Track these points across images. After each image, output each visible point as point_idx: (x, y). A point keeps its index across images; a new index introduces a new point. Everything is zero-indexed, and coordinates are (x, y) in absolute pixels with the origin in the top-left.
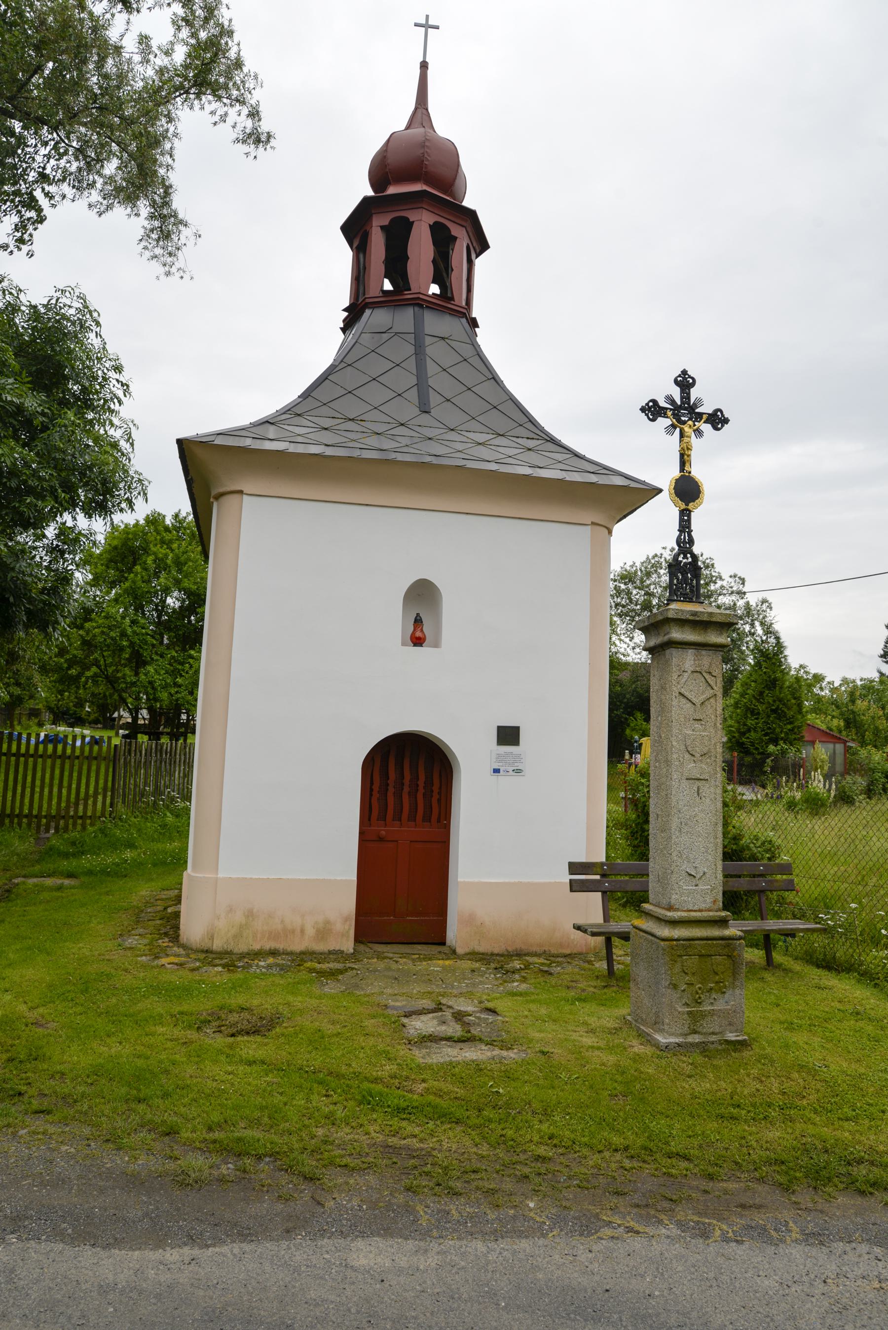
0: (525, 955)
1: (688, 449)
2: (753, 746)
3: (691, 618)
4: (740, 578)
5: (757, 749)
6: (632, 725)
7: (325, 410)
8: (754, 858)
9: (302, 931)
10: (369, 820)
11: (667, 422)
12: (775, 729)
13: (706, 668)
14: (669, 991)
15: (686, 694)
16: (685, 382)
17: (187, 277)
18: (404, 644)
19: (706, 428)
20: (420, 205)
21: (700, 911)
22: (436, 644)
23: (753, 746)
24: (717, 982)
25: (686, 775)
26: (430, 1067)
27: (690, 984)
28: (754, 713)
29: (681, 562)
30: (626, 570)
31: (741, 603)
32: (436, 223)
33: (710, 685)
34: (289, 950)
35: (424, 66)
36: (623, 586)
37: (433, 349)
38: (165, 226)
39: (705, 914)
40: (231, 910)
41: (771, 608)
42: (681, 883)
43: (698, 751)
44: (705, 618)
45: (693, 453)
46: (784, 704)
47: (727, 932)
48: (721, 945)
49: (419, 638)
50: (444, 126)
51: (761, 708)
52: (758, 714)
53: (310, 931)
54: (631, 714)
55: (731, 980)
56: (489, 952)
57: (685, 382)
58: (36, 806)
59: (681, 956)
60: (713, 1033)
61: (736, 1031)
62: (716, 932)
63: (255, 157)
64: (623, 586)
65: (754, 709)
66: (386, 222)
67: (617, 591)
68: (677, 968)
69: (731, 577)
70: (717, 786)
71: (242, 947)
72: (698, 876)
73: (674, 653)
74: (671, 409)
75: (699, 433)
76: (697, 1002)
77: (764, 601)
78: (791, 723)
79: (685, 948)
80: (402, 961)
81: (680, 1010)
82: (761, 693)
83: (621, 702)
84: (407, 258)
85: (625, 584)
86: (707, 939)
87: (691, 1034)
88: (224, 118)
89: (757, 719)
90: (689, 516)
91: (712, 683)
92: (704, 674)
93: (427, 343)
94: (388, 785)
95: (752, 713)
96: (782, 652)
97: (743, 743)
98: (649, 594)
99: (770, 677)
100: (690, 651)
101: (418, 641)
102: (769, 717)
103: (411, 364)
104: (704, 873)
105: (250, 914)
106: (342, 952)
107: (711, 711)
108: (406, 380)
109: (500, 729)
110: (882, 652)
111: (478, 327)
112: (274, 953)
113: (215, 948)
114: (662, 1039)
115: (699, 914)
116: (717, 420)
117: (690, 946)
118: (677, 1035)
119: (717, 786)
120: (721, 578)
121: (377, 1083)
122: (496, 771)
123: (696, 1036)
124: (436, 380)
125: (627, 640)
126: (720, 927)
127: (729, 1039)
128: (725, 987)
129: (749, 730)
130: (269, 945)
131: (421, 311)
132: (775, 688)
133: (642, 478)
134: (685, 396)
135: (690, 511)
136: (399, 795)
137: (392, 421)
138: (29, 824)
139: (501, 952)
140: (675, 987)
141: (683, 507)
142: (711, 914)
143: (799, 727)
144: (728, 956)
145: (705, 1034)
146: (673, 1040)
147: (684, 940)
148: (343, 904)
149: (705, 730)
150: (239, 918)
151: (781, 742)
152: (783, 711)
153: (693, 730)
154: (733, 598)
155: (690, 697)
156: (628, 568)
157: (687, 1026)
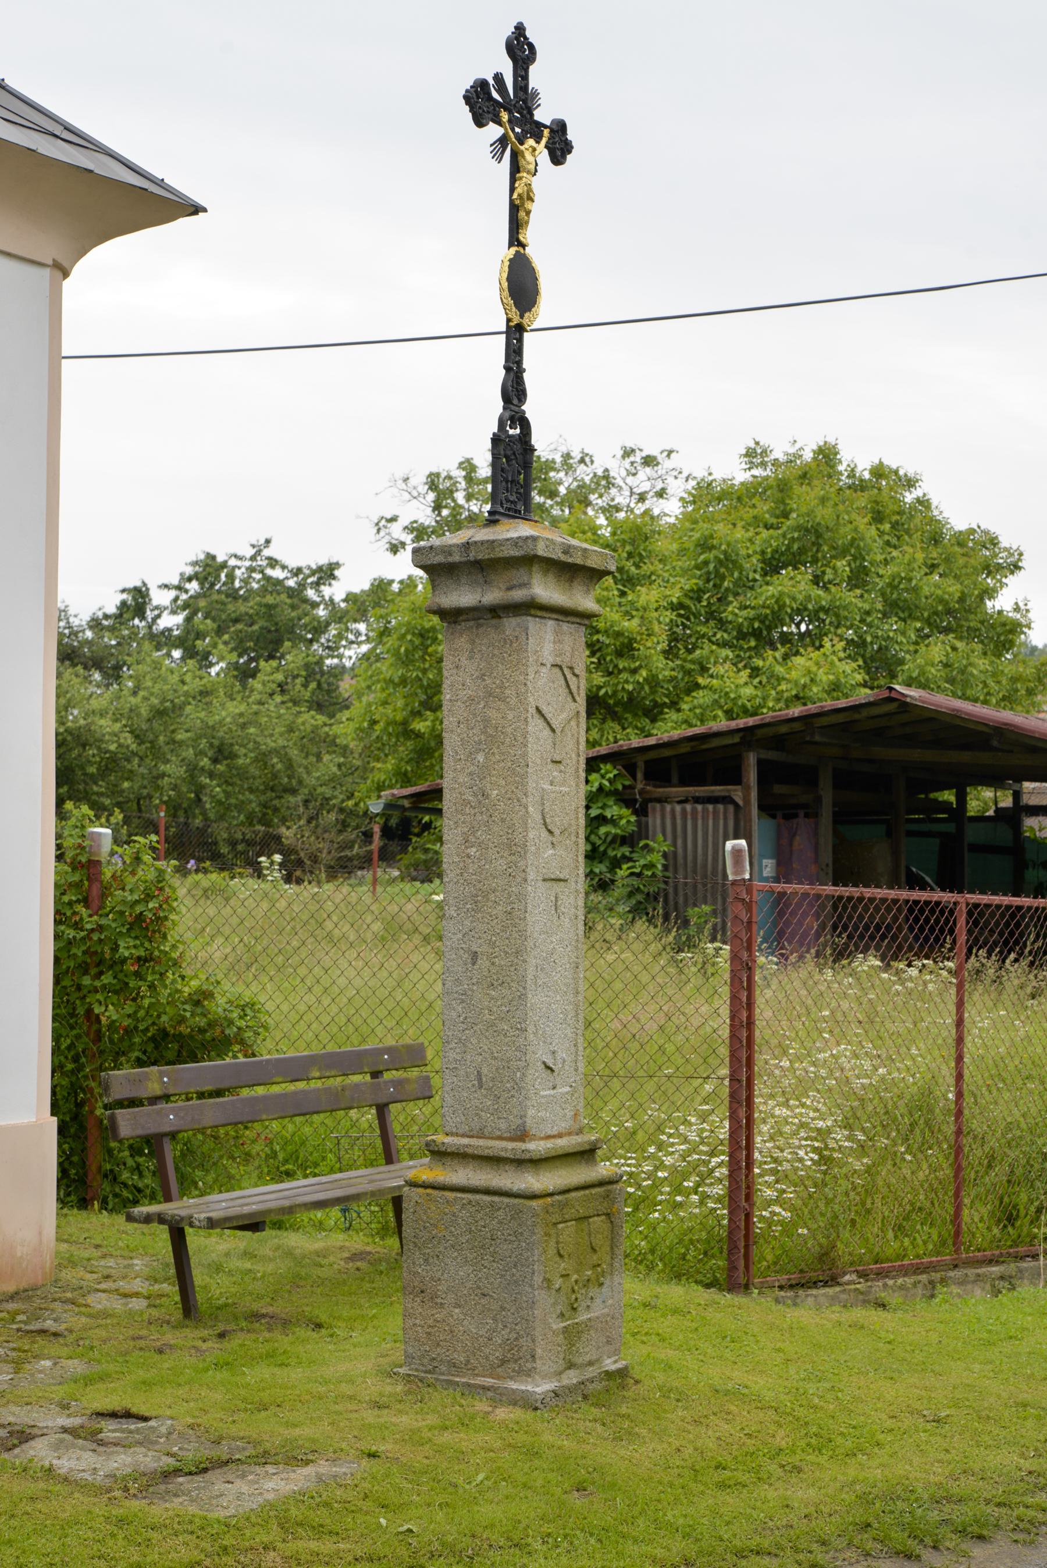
33: (571, 693)
45: (535, 208)
73: (531, 625)
86: (488, 1192)
91: (574, 688)
100: (550, 623)
110: (336, 573)
114: (541, 1387)
123: (571, 1373)
133: (158, 173)
147: (577, 1189)
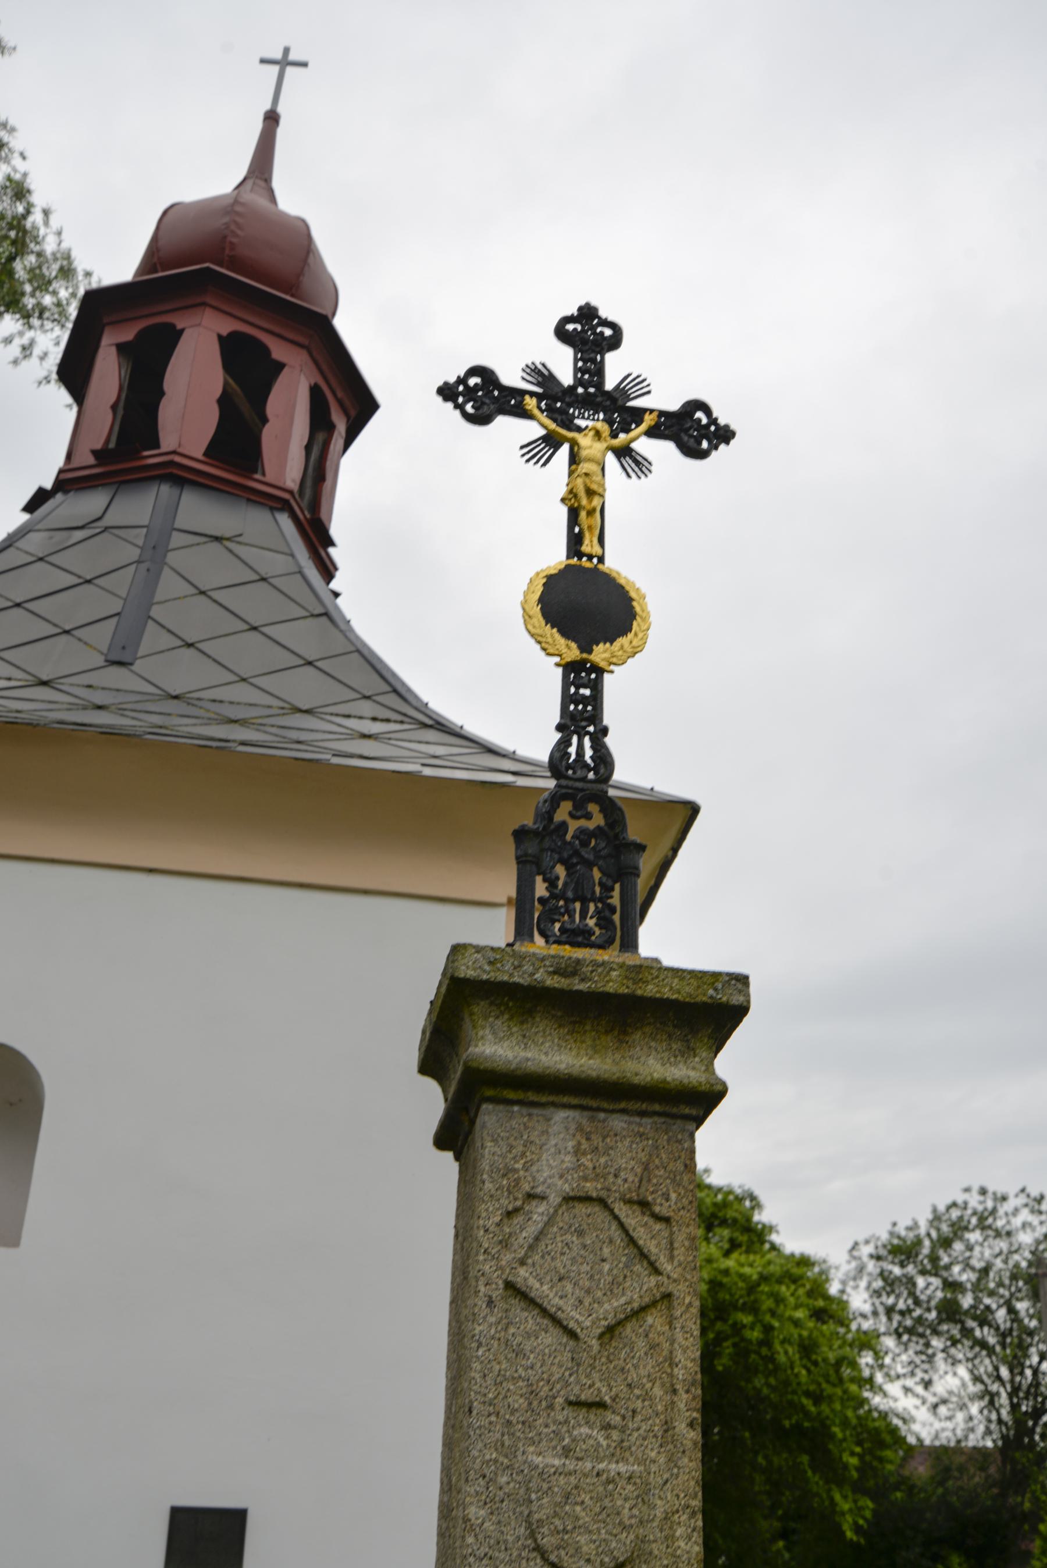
1: (590, 493)
11: (532, 430)
13: (627, 1181)
15: (540, 1289)
16: (589, 333)
19: (660, 452)
30: (899, 1237)
32: (233, 334)
35: (272, 119)
36: (897, 1271)
37: (188, 559)
50: (292, 196)
66: (128, 334)
67: (885, 1279)
75: (639, 465)
84: (162, 393)
85: (902, 1265)
88: (27, 350)
90: (597, 687)
91: (652, 1247)
92: (621, 1210)
98: (952, 1286)
100: (561, 1115)
107: (649, 1366)
111: (332, 543)
116: (694, 430)
125: (920, 1389)
131: (176, 491)
134: (591, 368)
135: (600, 671)
141: (572, 652)
149: (620, 1451)
153: (567, 1452)
156: (903, 1233)
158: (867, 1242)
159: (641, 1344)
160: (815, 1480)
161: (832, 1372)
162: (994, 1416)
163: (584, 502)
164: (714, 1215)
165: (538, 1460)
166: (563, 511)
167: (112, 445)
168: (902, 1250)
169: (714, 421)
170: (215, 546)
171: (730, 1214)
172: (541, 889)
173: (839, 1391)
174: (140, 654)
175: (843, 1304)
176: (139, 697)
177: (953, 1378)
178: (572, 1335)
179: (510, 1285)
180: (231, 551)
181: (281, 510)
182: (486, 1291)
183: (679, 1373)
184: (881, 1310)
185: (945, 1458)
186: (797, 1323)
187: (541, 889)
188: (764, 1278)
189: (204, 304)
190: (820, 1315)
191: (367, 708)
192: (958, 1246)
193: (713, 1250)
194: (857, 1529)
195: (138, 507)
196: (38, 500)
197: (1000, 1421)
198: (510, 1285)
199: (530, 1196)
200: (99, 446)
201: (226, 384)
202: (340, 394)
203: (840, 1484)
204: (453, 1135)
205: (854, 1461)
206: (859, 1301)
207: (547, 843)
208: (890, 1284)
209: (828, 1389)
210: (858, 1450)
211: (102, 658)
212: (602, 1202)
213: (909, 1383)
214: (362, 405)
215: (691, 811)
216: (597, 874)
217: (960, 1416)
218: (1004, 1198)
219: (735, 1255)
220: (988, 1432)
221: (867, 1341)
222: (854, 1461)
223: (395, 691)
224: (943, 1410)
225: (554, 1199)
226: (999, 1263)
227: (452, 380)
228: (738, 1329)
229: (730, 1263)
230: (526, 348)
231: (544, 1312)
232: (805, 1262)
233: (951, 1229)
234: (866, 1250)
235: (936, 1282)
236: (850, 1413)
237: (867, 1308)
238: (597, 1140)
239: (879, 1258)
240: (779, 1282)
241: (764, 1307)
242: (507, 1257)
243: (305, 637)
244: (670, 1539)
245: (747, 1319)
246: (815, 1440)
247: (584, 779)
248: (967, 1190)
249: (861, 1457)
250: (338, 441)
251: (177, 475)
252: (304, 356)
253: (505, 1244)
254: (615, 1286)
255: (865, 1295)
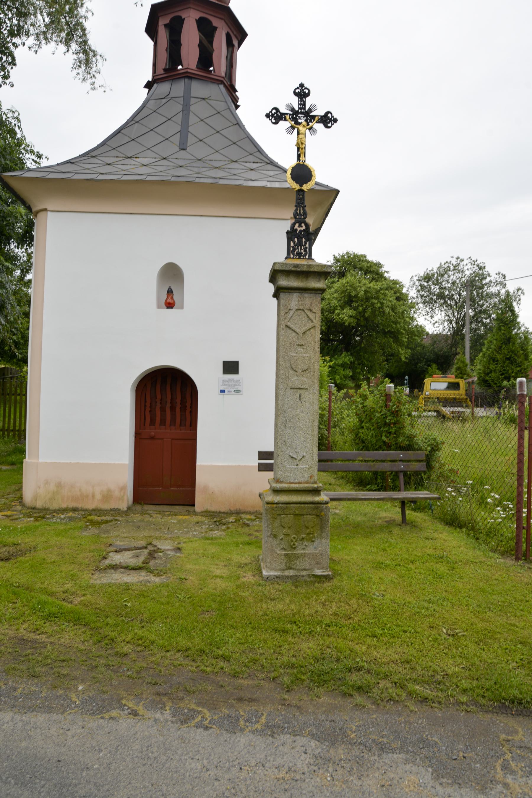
0: (242, 513)
1: (302, 143)
2: (493, 382)
3: (294, 269)
4: (502, 275)
5: (496, 384)
6: (430, 372)
7: (114, 153)
8: (420, 449)
9: (93, 496)
10: (144, 425)
12: (508, 370)
13: (308, 306)
14: (271, 539)
15: (291, 326)
17: (108, 90)
18: (159, 307)
19: (319, 127)
20: (188, 6)
21: (299, 483)
22: (182, 307)
23: (493, 382)
24: (308, 534)
25: (290, 385)
26: (93, 586)
27: (287, 535)
28: (495, 360)
29: (296, 230)
31: (503, 291)
33: (310, 319)
34: (85, 508)
36: (426, 284)
37: (196, 107)
38: (87, 57)
39: (302, 486)
40: (47, 483)
41: (523, 294)
42: (285, 464)
43: (300, 368)
44: (305, 269)
46: (515, 354)
47: (317, 499)
48: (311, 508)
49: (169, 303)
51: (499, 357)
52: (497, 361)
53: (98, 496)
54: (429, 365)
55: (319, 532)
56: (218, 510)
57: (302, 93)
58: (17, 424)
59: (280, 515)
60: (304, 570)
61: (323, 568)
62: (309, 498)
63: (142, 5)
64: (426, 284)
65: (494, 358)
68: (277, 523)
69: (496, 274)
70: (315, 393)
71: (55, 506)
72: (299, 459)
74: (290, 114)
76: (292, 547)
77: (519, 289)
78: (520, 366)
79: (283, 509)
80: (155, 516)
81: (279, 552)
82: (500, 348)
83: (424, 358)
85: (427, 282)
87: (286, 569)
89: (497, 364)
91: (312, 318)
92: (306, 311)
93: (192, 103)
94: (181, 404)
95: (494, 361)
96: (516, 320)
97: (487, 381)
99: (506, 336)
100: (295, 294)
101: (170, 305)
102: (504, 362)
103: (179, 119)
104: (303, 457)
105: (59, 485)
106: (119, 510)
108: (174, 127)
109: (224, 363)
111: (237, 91)
112: (75, 510)
113: (37, 506)
115: (297, 485)
116: (327, 120)
117: (287, 508)
118: (276, 570)
119: (315, 393)
120: (489, 275)
121: (52, 596)
122: (223, 391)
124: (196, 129)
125: (429, 319)
126: (313, 495)
127: (316, 574)
128: (314, 537)
129: (491, 372)
130: (72, 505)
131: (190, 81)
132: (509, 343)
134: (302, 104)
136: (163, 409)
137: (157, 156)
138: (14, 435)
139: (226, 511)
140: (275, 536)
142: (307, 485)
143: (525, 369)
144: (317, 515)
145: (298, 570)
146: (273, 573)
147: (282, 504)
148: (127, 478)
149: (306, 352)
150: (52, 487)
151: (512, 379)
152: (514, 359)
153: (297, 353)
154: (498, 288)
155: (294, 328)
157: (284, 564)
158: (416, 276)
159: (310, 335)
160: (394, 345)
161: (400, 315)
162: (451, 326)
163: (301, 146)
164: (367, 270)
165: (292, 354)
166: (296, 148)
167: (167, 67)
168: (427, 278)
169: (332, 117)
170: (203, 101)
171: (372, 269)
172: (292, 244)
173: (402, 321)
174: (188, 145)
175: (406, 295)
176: (191, 161)
177: (440, 315)
178: (297, 334)
179: (286, 326)
180: (208, 103)
181: (221, 84)
182: (283, 327)
183: (316, 339)
184: (419, 296)
185: (436, 338)
186: (390, 301)
187: (292, 244)
188: (381, 289)
189: (190, 8)
190: (398, 299)
191: (251, 158)
192: (446, 276)
193: (367, 282)
194: (406, 358)
195: (178, 88)
196: (149, 85)
197: (453, 327)
198: (286, 326)
199: (290, 310)
200: (164, 68)
201: (200, 36)
202: (235, 33)
203: (401, 347)
204: (276, 295)
205: (406, 340)
206: (413, 293)
207: (293, 234)
208: (422, 287)
209: (399, 320)
210: (407, 337)
211: (178, 148)
212: (303, 310)
213: (427, 317)
214: (242, 35)
215: (338, 192)
216: (304, 240)
217: (441, 326)
218: (462, 260)
219: (372, 283)
220: (449, 330)
221: (412, 306)
222: (406, 340)
223: (259, 151)
224: (436, 325)
225: (294, 310)
226: (458, 281)
227: (268, 112)
228: (373, 304)
229: (371, 285)
230: (287, 101)
231: (292, 330)
232: (395, 282)
233: (444, 271)
234: (415, 278)
235: (437, 287)
236: (406, 327)
237: (415, 296)
238: (302, 299)
239: (419, 280)
240: (386, 290)
241: (381, 298)
242: (286, 321)
243: (231, 133)
244: (314, 366)
245: (376, 301)
246: (395, 335)
247: (301, 218)
248: (452, 257)
249: (408, 339)
250: (235, 49)
251: (188, 76)
252: (223, 23)
253: (285, 318)
254: (305, 325)
255: (415, 291)
